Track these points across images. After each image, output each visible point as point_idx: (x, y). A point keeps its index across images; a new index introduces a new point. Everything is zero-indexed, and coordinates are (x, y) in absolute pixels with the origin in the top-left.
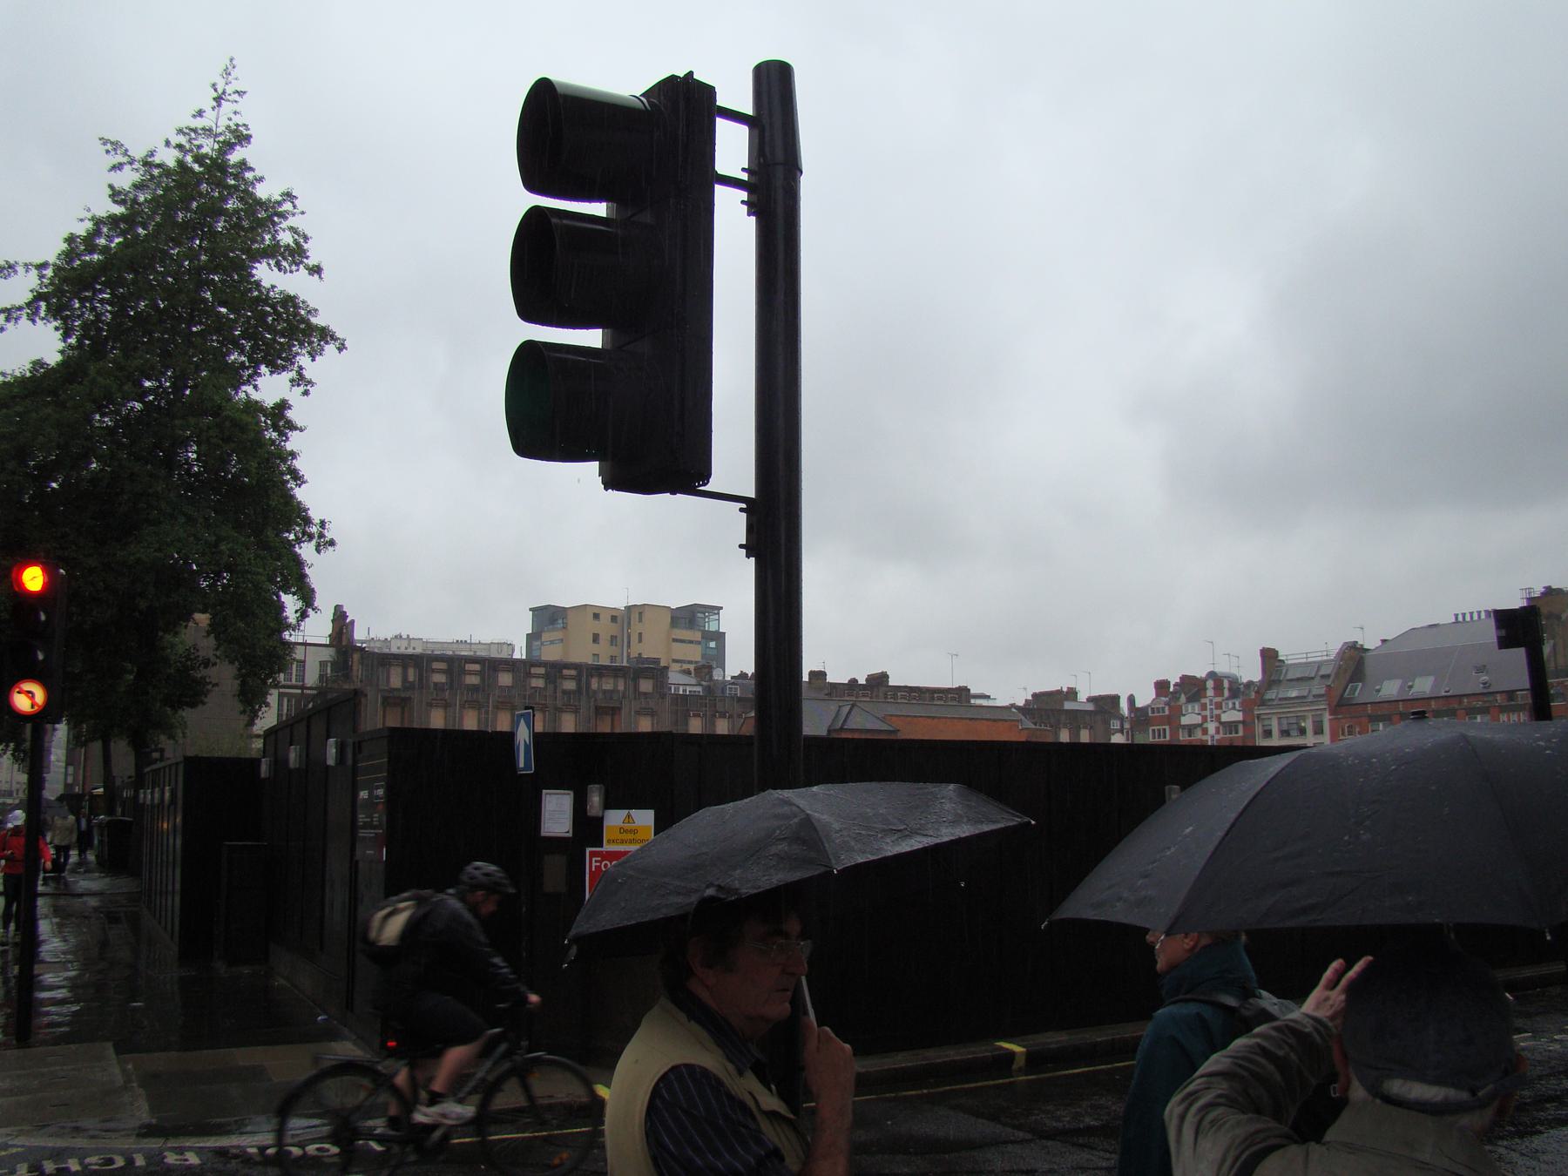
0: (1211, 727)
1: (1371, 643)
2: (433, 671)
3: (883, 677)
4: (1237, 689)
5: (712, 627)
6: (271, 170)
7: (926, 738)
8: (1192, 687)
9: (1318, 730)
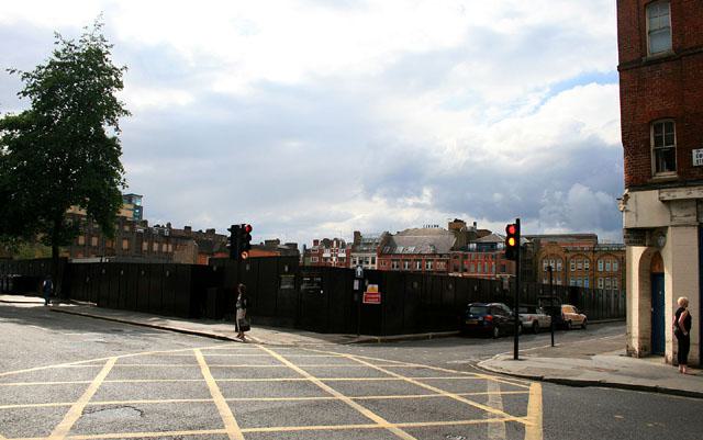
0: (334, 259)
1: (393, 233)
2: (604, 270)
3: (213, 230)
4: (341, 244)
5: (138, 204)
6: (114, 60)
7: (698, 289)
8: (327, 243)
9: (373, 262)
